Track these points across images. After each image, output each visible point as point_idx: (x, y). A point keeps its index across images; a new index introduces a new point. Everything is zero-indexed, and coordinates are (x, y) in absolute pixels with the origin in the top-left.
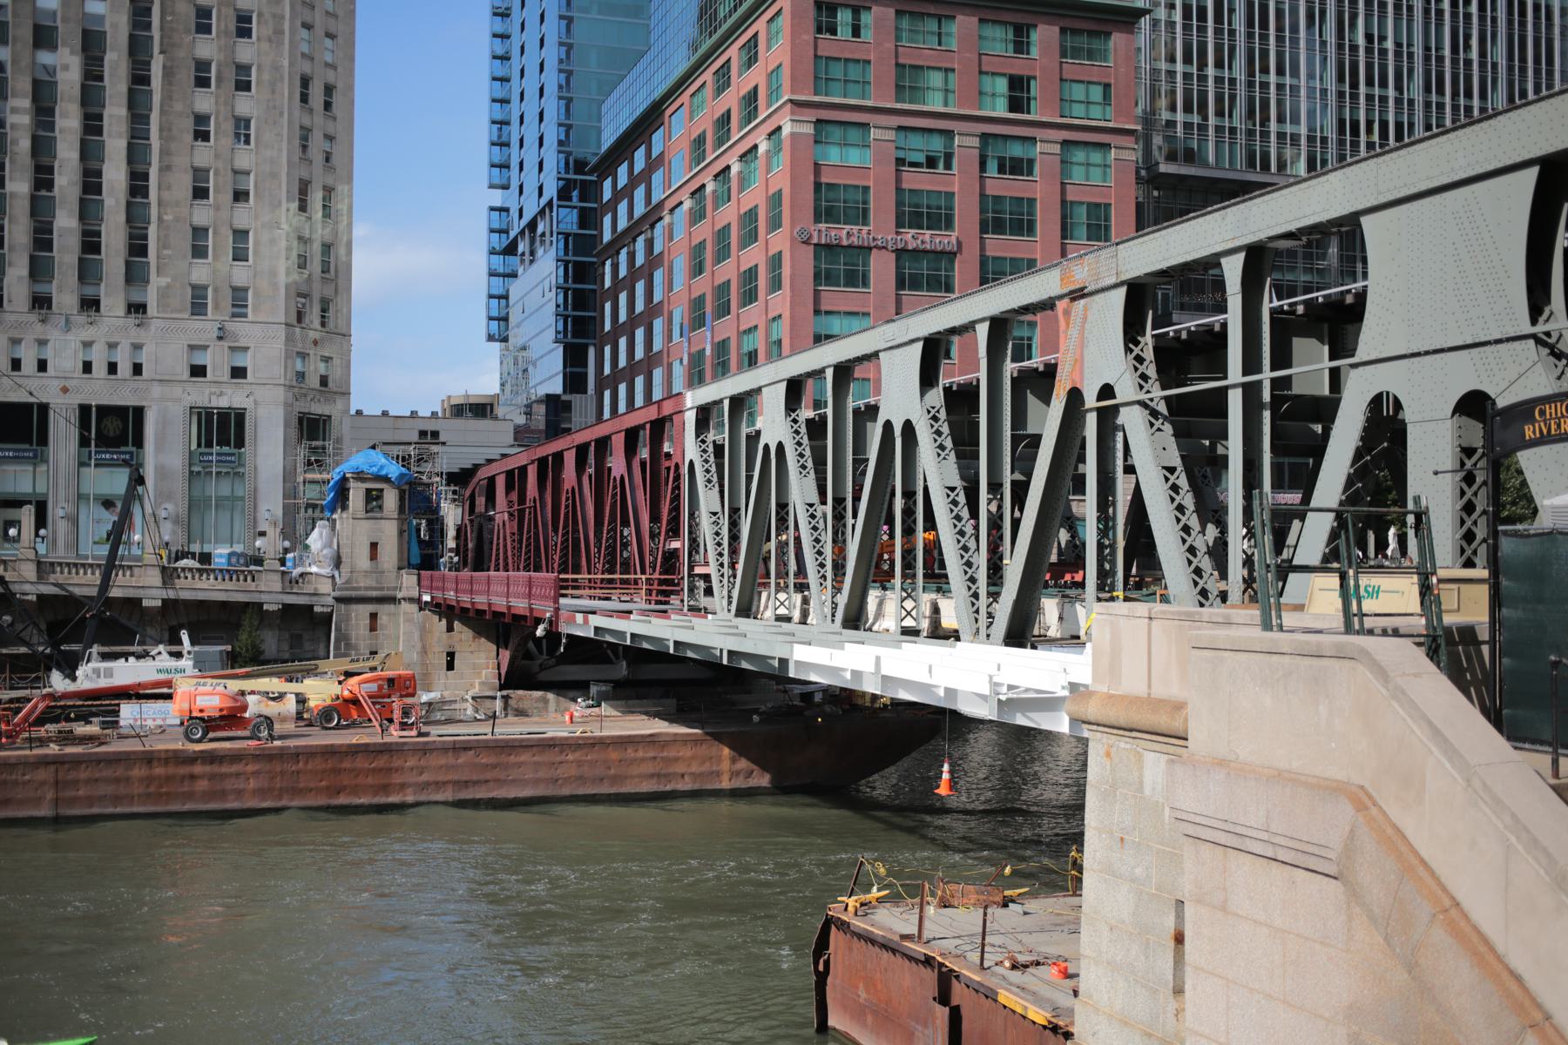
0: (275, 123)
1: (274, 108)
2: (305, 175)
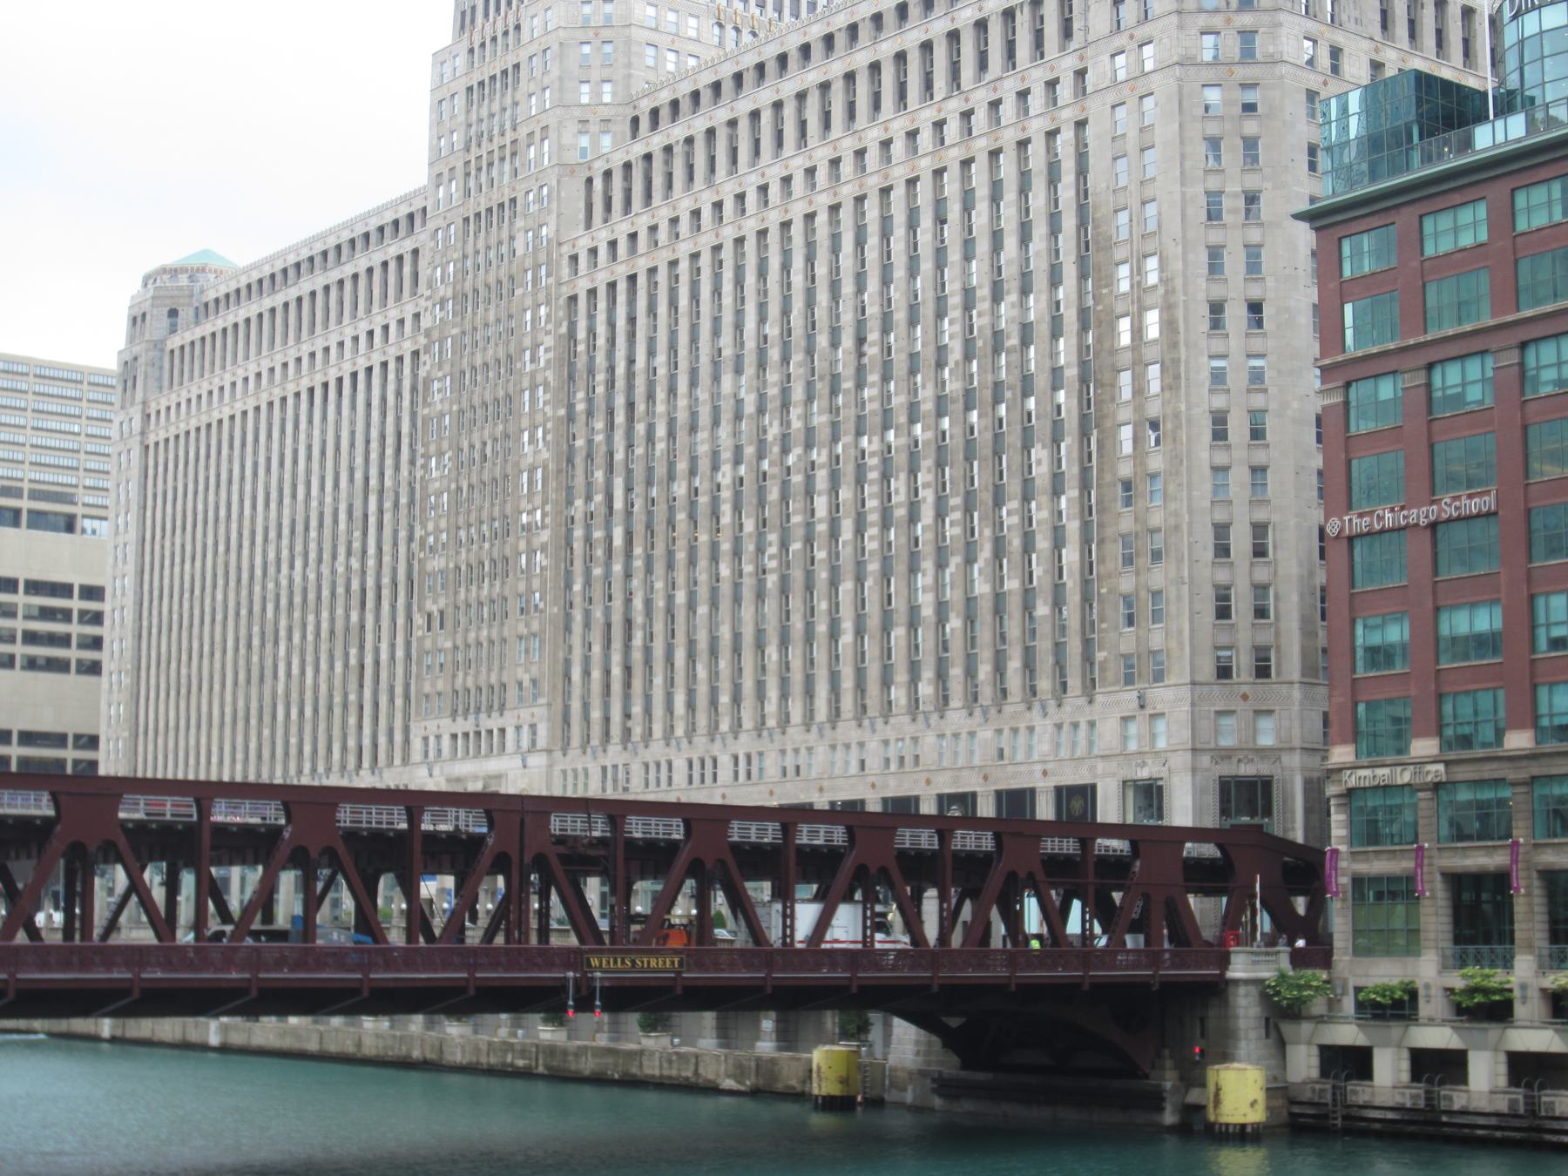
1: (1176, 457)
2: (1220, 516)
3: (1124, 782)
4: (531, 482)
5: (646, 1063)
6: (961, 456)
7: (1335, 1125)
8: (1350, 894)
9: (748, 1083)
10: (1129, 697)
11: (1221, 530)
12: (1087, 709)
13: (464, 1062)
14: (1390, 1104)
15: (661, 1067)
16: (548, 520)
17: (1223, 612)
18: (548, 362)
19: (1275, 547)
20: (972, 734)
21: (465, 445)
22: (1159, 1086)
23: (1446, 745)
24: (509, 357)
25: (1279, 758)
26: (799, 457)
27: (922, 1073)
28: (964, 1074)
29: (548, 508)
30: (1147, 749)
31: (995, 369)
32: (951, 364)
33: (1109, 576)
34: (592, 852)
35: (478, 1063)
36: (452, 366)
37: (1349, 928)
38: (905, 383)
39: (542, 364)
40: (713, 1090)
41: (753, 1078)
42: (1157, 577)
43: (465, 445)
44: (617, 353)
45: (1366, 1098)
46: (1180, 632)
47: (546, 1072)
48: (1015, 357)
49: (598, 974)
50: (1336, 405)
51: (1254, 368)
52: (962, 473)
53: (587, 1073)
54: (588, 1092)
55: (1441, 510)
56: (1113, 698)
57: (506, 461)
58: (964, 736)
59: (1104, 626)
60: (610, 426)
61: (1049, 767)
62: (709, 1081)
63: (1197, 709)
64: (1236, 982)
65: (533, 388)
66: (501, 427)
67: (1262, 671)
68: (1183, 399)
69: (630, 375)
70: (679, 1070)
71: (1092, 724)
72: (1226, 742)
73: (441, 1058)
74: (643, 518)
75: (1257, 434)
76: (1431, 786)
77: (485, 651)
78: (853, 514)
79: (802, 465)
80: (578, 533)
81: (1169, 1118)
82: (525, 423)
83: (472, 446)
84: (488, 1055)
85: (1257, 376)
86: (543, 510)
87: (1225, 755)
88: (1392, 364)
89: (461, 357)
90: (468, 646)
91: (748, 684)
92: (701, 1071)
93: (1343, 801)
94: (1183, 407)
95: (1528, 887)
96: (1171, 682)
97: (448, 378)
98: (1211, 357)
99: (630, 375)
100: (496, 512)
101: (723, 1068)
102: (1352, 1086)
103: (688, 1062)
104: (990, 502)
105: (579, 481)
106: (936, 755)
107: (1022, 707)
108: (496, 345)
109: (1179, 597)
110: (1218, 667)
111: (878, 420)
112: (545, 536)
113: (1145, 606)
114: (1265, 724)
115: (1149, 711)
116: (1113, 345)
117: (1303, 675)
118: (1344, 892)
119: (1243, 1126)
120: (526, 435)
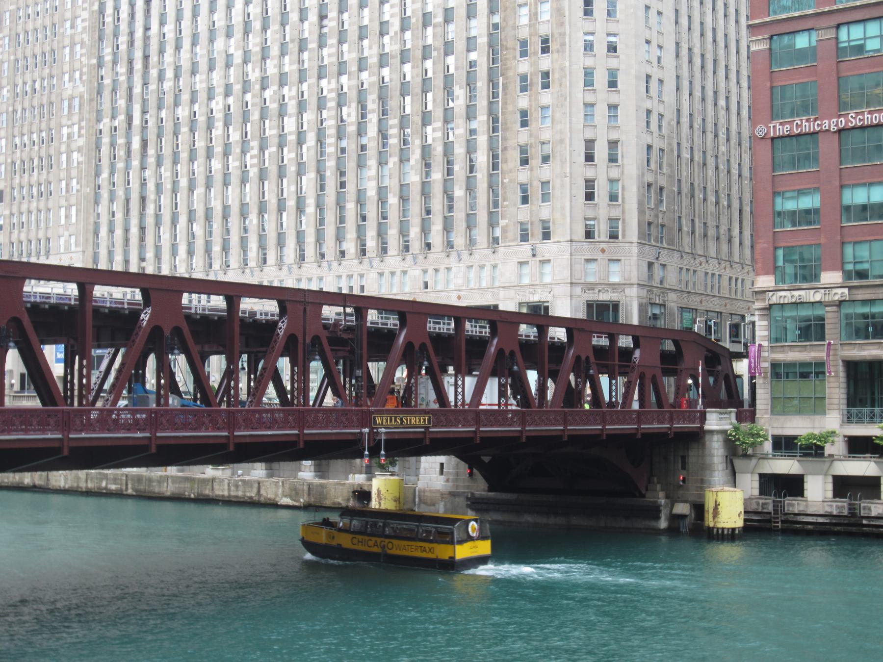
0: (562, 106)
1: (562, 95)
2: (589, 135)
3: (520, 304)
4: (70, 107)
5: (216, 487)
6: (398, 93)
7: (778, 526)
8: (769, 374)
9: (302, 500)
10: (524, 250)
11: (589, 144)
12: (492, 256)
13: (67, 487)
14: (821, 512)
15: (229, 489)
16: (83, 132)
17: (589, 196)
18: (84, 28)
19: (622, 156)
20: (404, 273)
21: (20, 82)
22: (656, 502)
23: (848, 275)
24: (54, 25)
25: (624, 290)
26: (275, 92)
27: (453, 494)
28: (492, 494)
29: (83, 124)
30: (537, 283)
31: (424, 37)
32: (392, 33)
33: (511, 171)
34: (345, 336)
35: (78, 487)
36: (10, 30)
37: (769, 396)
38: (356, 45)
39: (79, 29)
40: (274, 505)
41: (306, 498)
42: (546, 172)
43: (20, 82)
44: (137, 24)
45: (801, 508)
46: (563, 208)
47: (134, 493)
48: (440, 30)
49: (383, 430)
50: (764, 50)
51: (611, 42)
52: (399, 103)
53: (168, 494)
54: (168, 506)
55: (847, 121)
56: (511, 249)
57: (51, 93)
58: (398, 273)
59: (505, 203)
60: (131, 70)
61: (462, 294)
62: (270, 499)
63: (573, 257)
64: (711, 432)
65: (72, 45)
66: (47, 71)
67: (613, 236)
68: (567, 59)
69: (146, 39)
70: (245, 492)
71: (494, 266)
72: (591, 279)
73: (47, 484)
74: (155, 131)
75: (613, 84)
76: (837, 303)
77: (33, 217)
78: (316, 130)
79: (277, 97)
80: (106, 140)
81: (663, 524)
82: (66, 68)
83: (25, 83)
84: (87, 482)
85: (612, 48)
86: (80, 124)
87: (590, 287)
88: (809, 24)
89: (17, 24)
90: (21, 213)
91: (234, 239)
92: (263, 492)
93: (765, 312)
94: (567, 64)
95: (836, 372)
96: (556, 240)
97: (7, 39)
98: (585, 34)
99: (146, 39)
100: (44, 126)
101: (280, 490)
102: (788, 501)
103: (251, 486)
104: (420, 123)
105: (106, 106)
106: (377, 286)
107: (444, 255)
108: (44, 17)
109: (562, 186)
110: (586, 231)
111: (335, 69)
112: (81, 142)
113: (535, 193)
114: (615, 268)
115: (538, 258)
116: (515, 23)
117: (639, 238)
118: (765, 373)
119: (733, 529)
120: (66, 77)
